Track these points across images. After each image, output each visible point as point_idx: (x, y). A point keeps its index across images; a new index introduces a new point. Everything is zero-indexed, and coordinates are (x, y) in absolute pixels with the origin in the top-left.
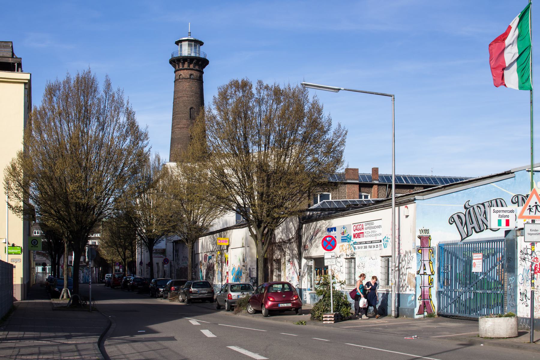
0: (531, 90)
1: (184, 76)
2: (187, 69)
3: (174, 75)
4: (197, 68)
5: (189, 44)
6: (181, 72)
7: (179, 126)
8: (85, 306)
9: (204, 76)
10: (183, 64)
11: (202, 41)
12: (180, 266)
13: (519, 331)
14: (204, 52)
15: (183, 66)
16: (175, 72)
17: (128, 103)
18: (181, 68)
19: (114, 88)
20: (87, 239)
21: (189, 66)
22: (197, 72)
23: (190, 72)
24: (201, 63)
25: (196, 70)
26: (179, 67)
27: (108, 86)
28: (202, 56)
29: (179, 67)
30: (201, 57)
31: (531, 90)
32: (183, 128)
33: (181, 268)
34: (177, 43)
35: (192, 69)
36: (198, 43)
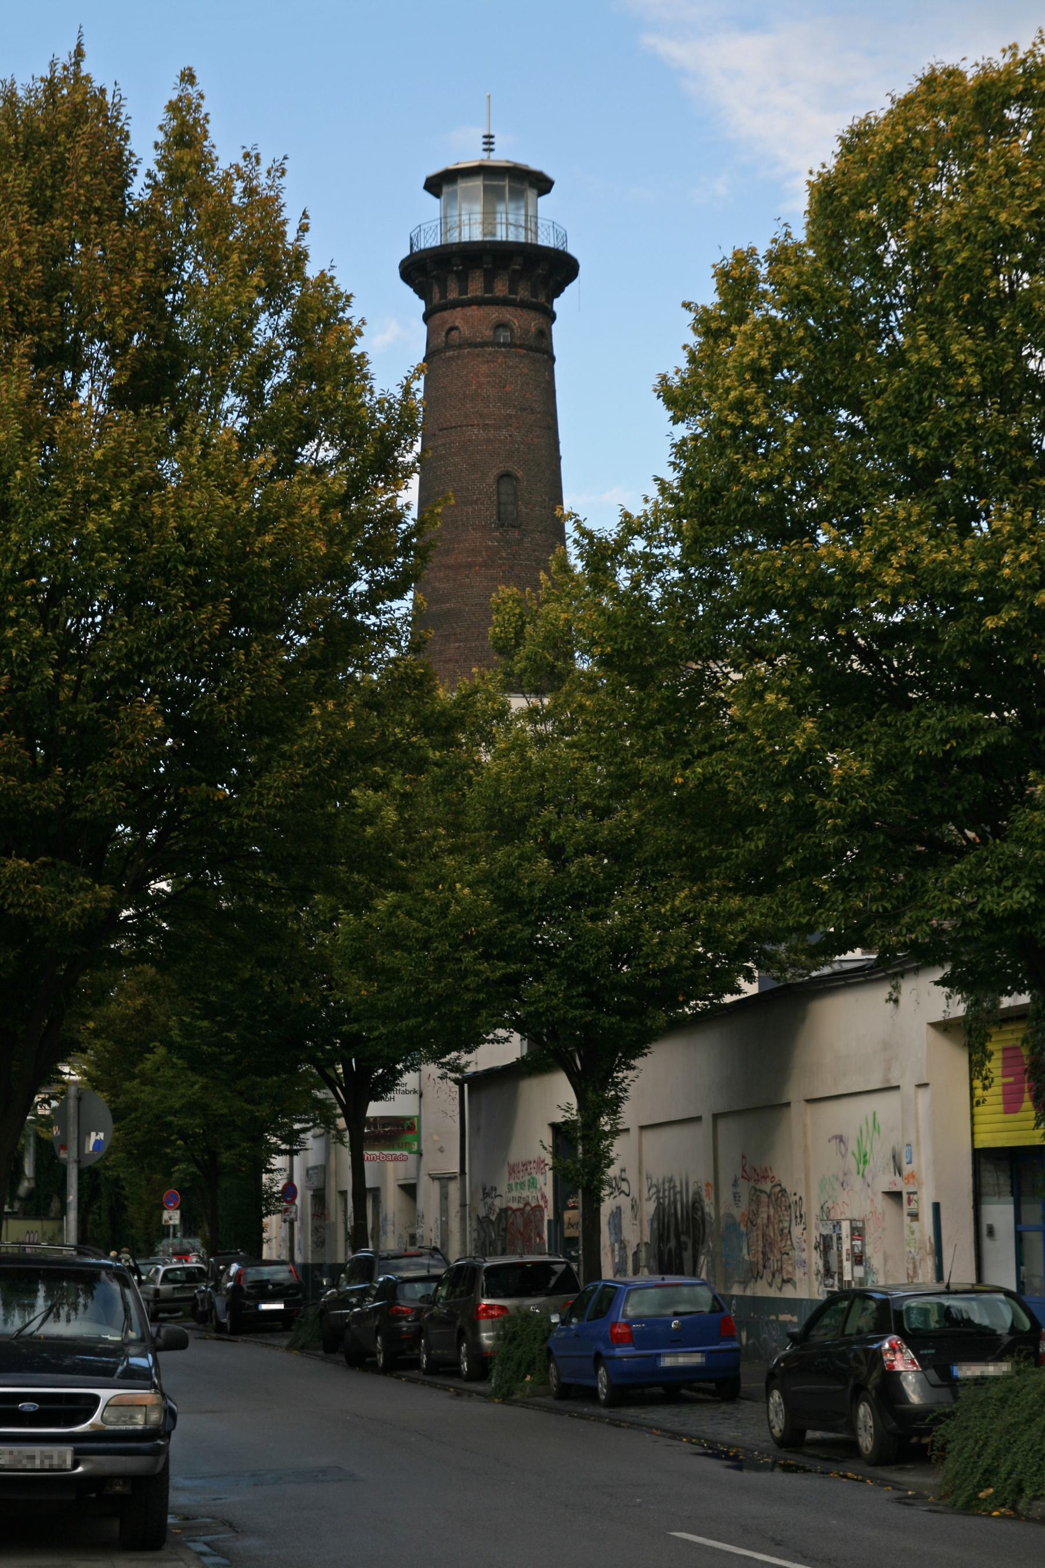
0: (421, 1096)
1: (466, 332)
2: (480, 302)
3: (424, 328)
4: (523, 293)
5: (486, 189)
6: (456, 317)
7: (451, 560)
8: (189, 1548)
9: (562, 336)
10: (463, 279)
11: (550, 173)
12: (499, 1203)
13: (563, 1380)
14: (551, 221)
15: (464, 290)
16: (426, 318)
17: (304, 229)
18: (453, 295)
19: (225, 150)
20: (28, 1106)
21: (488, 287)
23: (495, 314)
24: (557, 269)
25: (523, 305)
26: (443, 295)
27: (185, 134)
28: (546, 239)
29: (443, 295)
30: (540, 243)
31: (421, 1096)
32: (469, 566)
33: (504, 1211)
34: (435, 185)
35: (504, 302)
36: (202, 97)
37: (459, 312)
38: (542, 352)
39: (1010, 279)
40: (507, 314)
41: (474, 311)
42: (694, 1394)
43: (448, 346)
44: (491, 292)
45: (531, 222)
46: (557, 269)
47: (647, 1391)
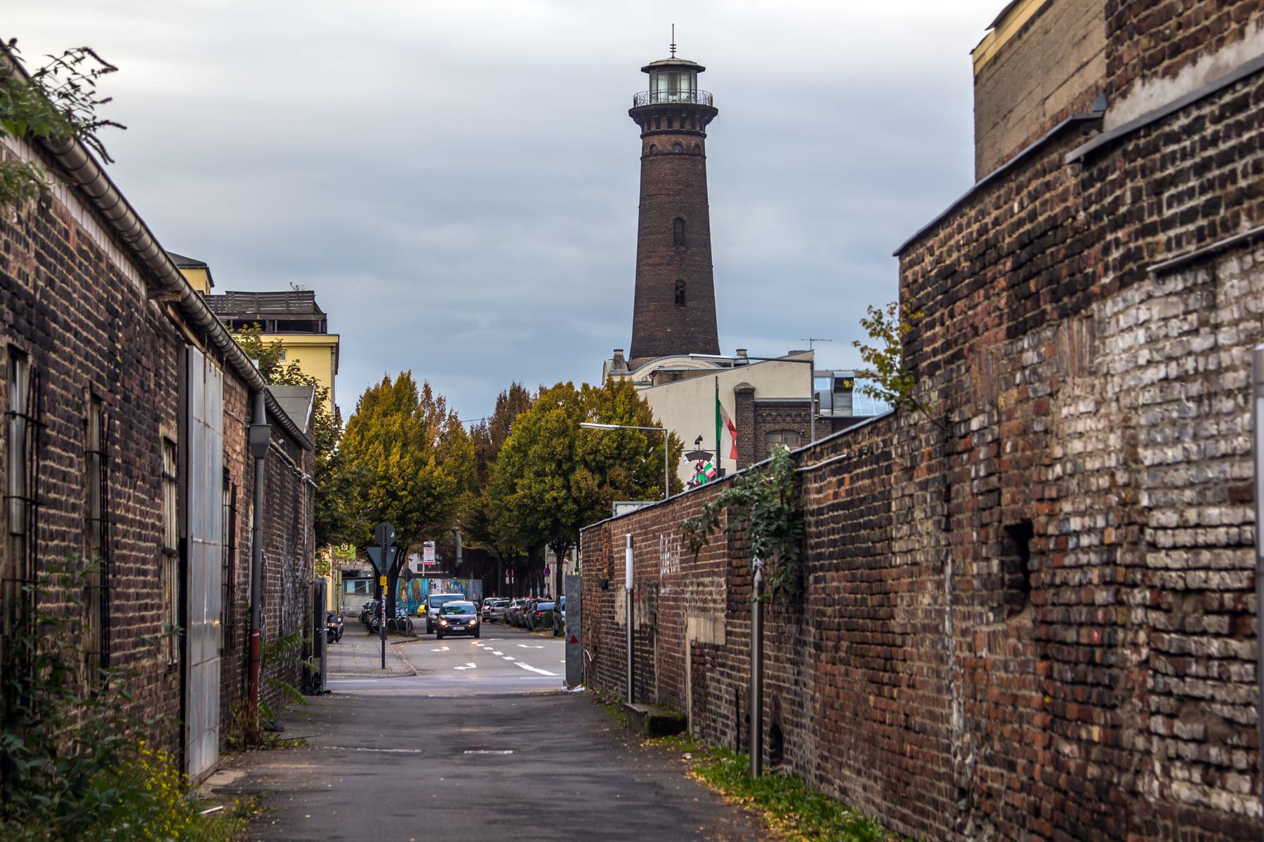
1: (660, 148)
2: (666, 133)
6: (655, 140)
7: (651, 261)
15: (658, 127)
16: (642, 137)
18: (653, 129)
21: (670, 126)
22: (688, 138)
23: (673, 138)
24: (709, 112)
32: (660, 264)
37: (656, 137)
38: (697, 155)
39: (1089, 564)
40: (680, 138)
41: (663, 137)
42: (303, 511)
43: (651, 154)
44: (674, 94)
45: (693, 91)
46: (709, 112)
47: (177, 319)
